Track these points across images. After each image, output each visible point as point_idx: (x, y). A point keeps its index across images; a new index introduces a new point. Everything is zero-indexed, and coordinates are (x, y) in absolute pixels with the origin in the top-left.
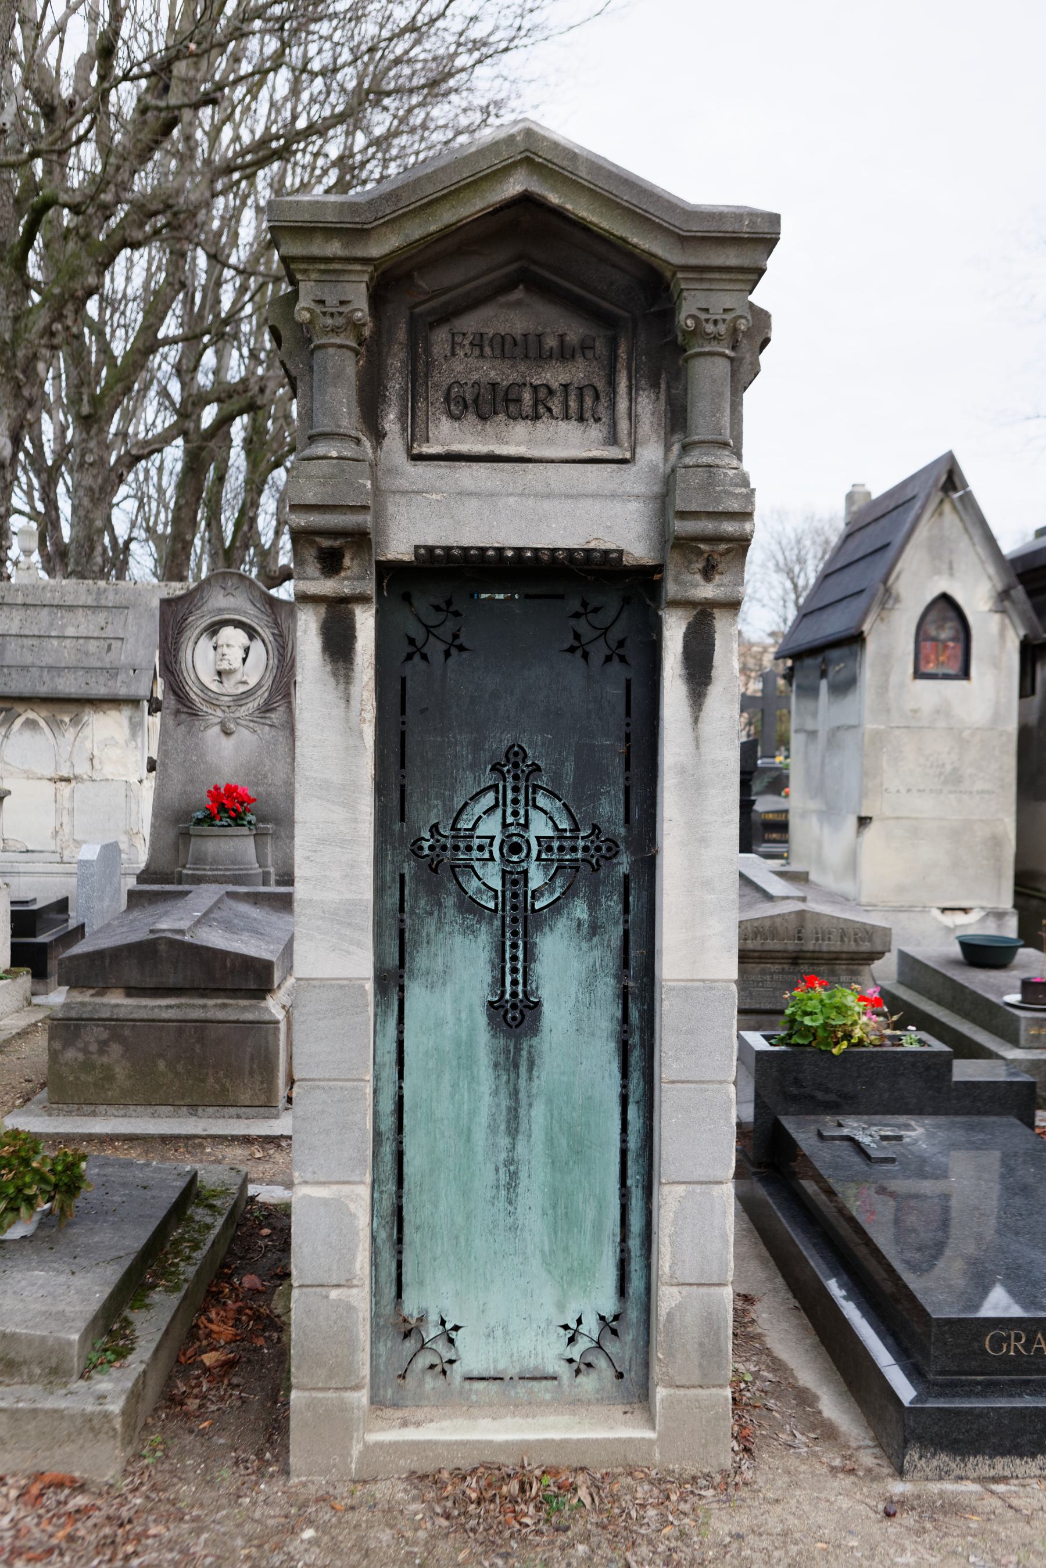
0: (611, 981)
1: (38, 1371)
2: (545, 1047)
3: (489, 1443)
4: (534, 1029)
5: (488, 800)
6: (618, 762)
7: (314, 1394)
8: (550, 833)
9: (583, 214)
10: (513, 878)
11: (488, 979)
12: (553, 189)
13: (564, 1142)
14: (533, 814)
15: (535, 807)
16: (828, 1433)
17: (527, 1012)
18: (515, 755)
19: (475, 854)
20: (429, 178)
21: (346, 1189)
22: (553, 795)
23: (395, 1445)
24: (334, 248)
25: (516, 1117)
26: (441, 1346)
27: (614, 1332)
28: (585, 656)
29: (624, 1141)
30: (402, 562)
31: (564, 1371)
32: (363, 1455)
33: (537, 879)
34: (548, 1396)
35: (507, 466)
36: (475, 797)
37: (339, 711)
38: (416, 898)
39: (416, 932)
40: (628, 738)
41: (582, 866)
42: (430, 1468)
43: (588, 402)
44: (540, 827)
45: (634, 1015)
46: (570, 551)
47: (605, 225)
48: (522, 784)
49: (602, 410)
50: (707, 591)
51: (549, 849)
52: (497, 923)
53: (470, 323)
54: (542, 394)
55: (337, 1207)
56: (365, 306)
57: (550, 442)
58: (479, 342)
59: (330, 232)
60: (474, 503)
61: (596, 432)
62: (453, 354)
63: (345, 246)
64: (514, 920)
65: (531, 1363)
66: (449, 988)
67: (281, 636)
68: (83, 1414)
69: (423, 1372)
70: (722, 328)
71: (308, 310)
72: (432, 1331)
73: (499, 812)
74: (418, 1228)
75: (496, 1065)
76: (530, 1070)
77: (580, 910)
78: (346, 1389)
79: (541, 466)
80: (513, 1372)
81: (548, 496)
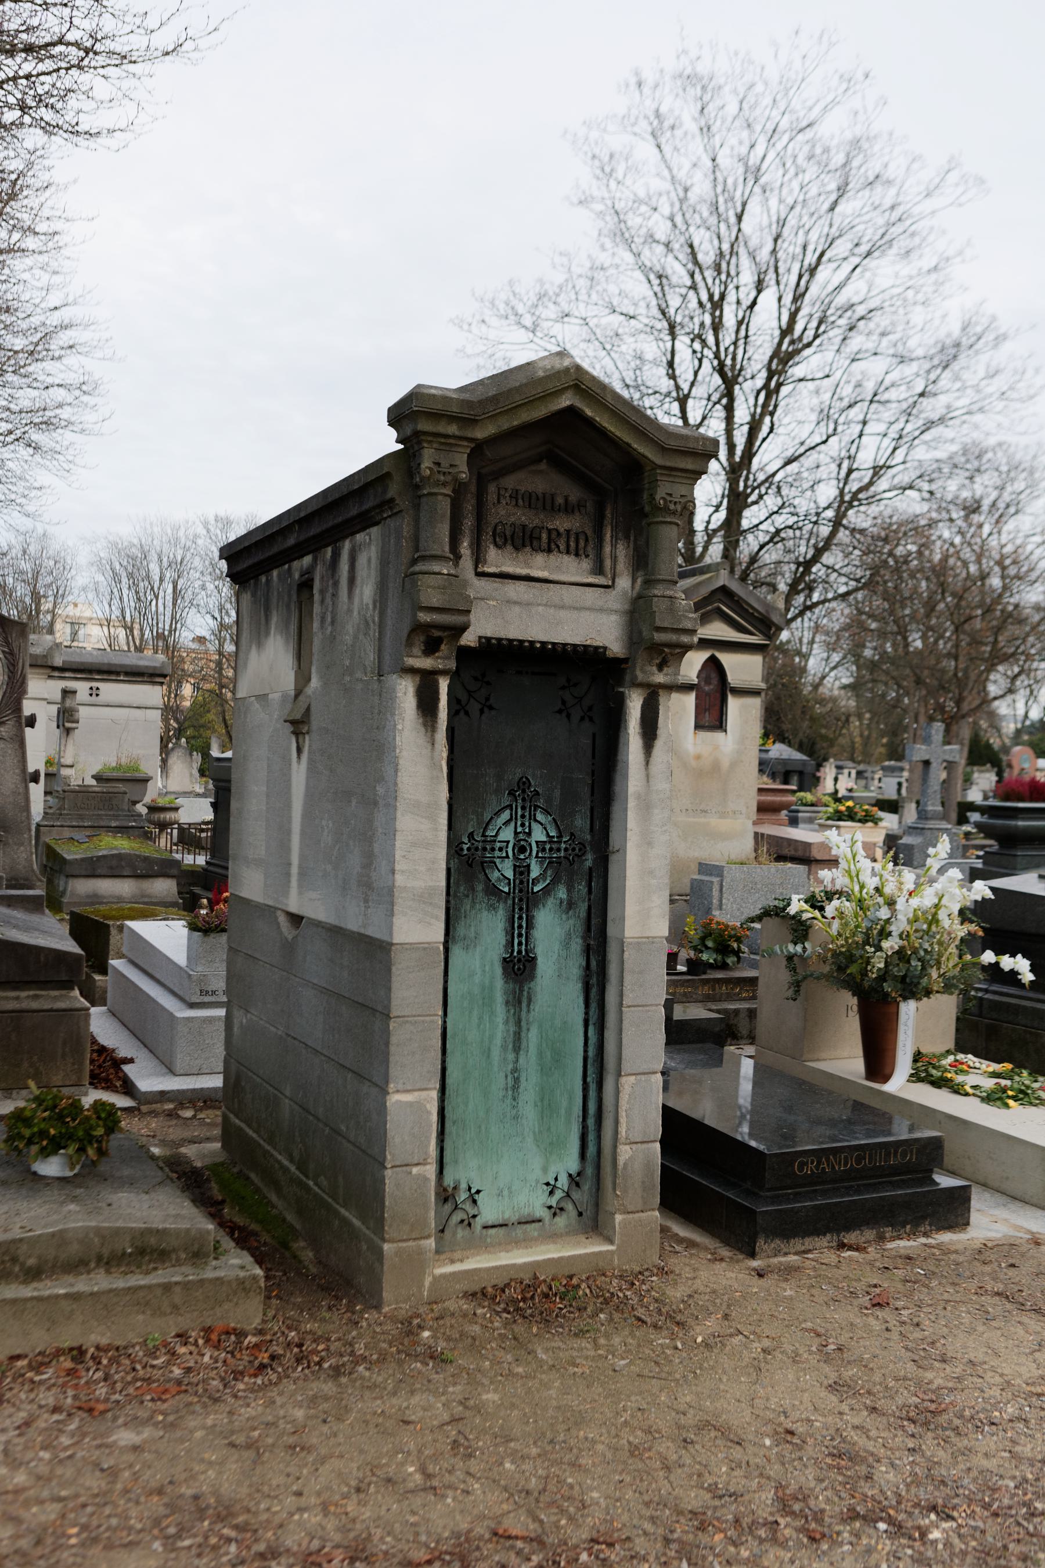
0: (580, 941)
1: (183, 1256)
2: (538, 988)
3: (514, 1265)
4: (532, 977)
5: (506, 815)
6: (587, 790)
7: (401, 1244)
8: (544, 838)
9: (606, 425)
10: (521, 871)
11: (503, 942)
12: (589, 406)
13: (548, 1054)
14: (534, 825)
15: (536, 820)
16: (691, 1244)
17: (528, 965)
18: (523, 784)
19: (497, 853)
20: (517, 390)
21: (424, 1094)
22: (547, 812)
23: (454, 1274)
24: (453, 429)
25: (519, 1039)
26: (468, 1206)
27: (578, 1185)
28: (568, 716)
29: (586, 1051)
30: (470, 647)
31: (545, 1214)
32: (432, 1284)
33: (535, 871)
34: (536, 1234)
35: (538, 585)
36: (498, 814)
37: (426, 751)
38: (457, 884)
39: (457, 909)
40: (593, 772)
41: (564, 862)
42: (476, 1287)
43: (582, 543)
44: (538, 835)
45: (594, 964)
46: (575, 646)
47: (618, 433)
48: (528, 804)
49: (590, 550)
50: (660, 678)
51: (544, 850)
52: (510, 902)
53: (510, 482)
54: (554, 535)
55: (418, 1107)
56: (465, 469)
57: (558, 569)
58: (515, 496)
59: (452, 418)
60: (517, 609)
61: (586, 564)
62: (499, 502)
63: (460, 428)
64: (521, 900)
65: (526, 1211)
66: (478, 949)
67: (11, 653)
68: (237, 1279)
69: (456, 1226)
70: (679, 508)
71: (430, 469)
72: (463, 1196)
73: (513, 824)
74: (454, 1123)
75: (507, 1003)
76: (528, 1005)
77: (562, 893)
78: (422, 1238)
79: (558, 586)
80: (514, 1219)
81: (563, 607)
